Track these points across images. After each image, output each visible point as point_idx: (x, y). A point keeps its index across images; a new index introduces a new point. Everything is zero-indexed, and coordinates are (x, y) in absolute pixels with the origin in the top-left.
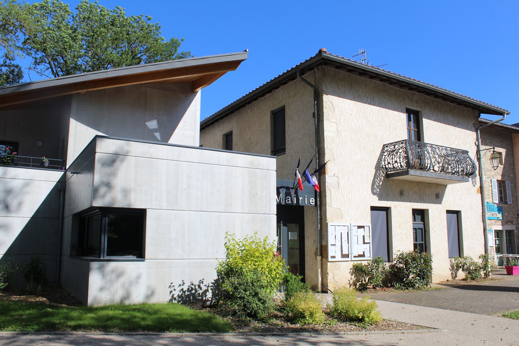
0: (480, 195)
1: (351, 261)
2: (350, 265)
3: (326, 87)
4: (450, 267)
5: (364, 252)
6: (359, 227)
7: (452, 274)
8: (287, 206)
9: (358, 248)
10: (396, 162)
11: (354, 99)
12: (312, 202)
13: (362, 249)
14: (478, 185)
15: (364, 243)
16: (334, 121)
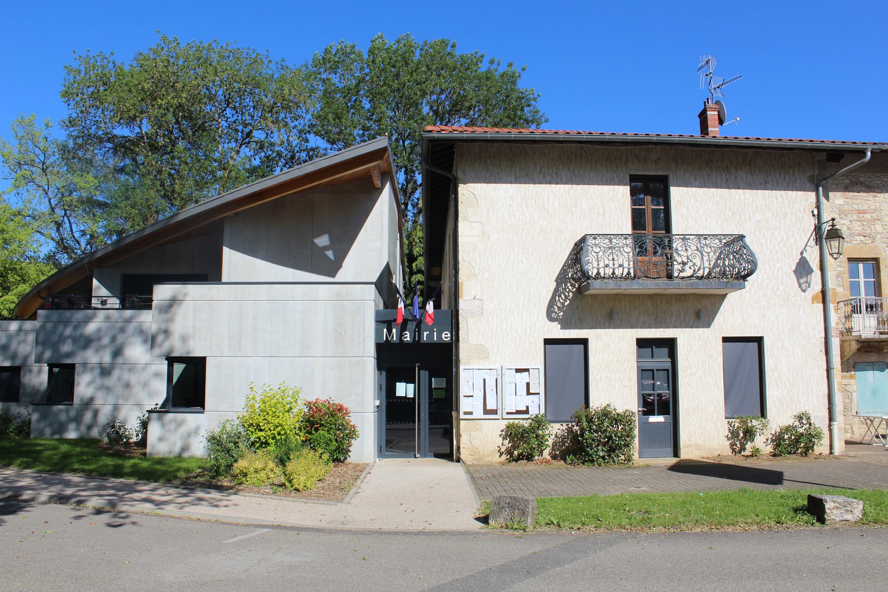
0: (821, 305)
2: (503, 424)
3: (464, 173)
4: (727, 433)
5: (527, 407)
6: (518, 371)
7: (732, 445)
9: (515, 401)
10: (620, 266)
11: (517, 181)
15: (528, 393)
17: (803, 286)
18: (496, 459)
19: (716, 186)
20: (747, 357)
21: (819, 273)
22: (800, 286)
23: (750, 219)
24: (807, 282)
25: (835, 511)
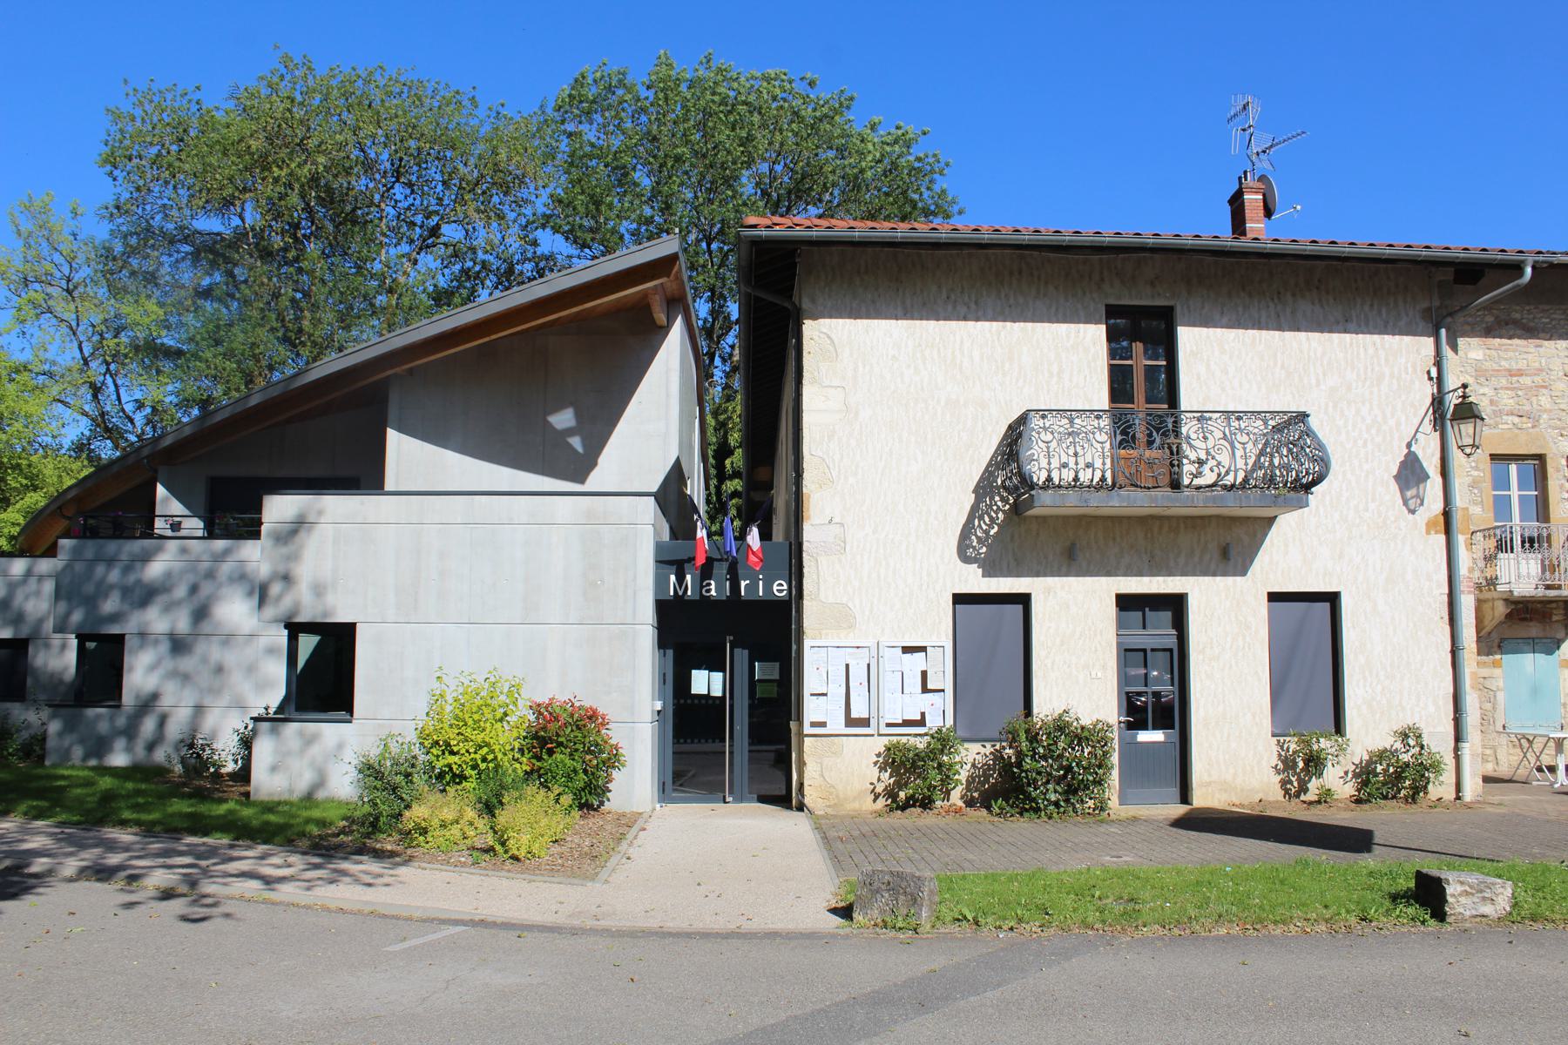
2: (880, 744)
3: (813, 301)
4: (1274, 760)
5: (923, 714)
6: (907, 650)
7: (1284, 783)
8: (679, 599)
9: (900, 703)
10: (1088, 465)
11: (907, 314)
13: (916, 699)
14: (1434, 504)
15: (925, 690)
16: (835, 383)
17: (1412, 503)
18: (868, 804)
19: (1384, 329)
20: (1311, 628)
21: (1439, 480)
22: (1405, 503)
23: (1318, 384)
24: (1417, 496)
25: (1463, 900)
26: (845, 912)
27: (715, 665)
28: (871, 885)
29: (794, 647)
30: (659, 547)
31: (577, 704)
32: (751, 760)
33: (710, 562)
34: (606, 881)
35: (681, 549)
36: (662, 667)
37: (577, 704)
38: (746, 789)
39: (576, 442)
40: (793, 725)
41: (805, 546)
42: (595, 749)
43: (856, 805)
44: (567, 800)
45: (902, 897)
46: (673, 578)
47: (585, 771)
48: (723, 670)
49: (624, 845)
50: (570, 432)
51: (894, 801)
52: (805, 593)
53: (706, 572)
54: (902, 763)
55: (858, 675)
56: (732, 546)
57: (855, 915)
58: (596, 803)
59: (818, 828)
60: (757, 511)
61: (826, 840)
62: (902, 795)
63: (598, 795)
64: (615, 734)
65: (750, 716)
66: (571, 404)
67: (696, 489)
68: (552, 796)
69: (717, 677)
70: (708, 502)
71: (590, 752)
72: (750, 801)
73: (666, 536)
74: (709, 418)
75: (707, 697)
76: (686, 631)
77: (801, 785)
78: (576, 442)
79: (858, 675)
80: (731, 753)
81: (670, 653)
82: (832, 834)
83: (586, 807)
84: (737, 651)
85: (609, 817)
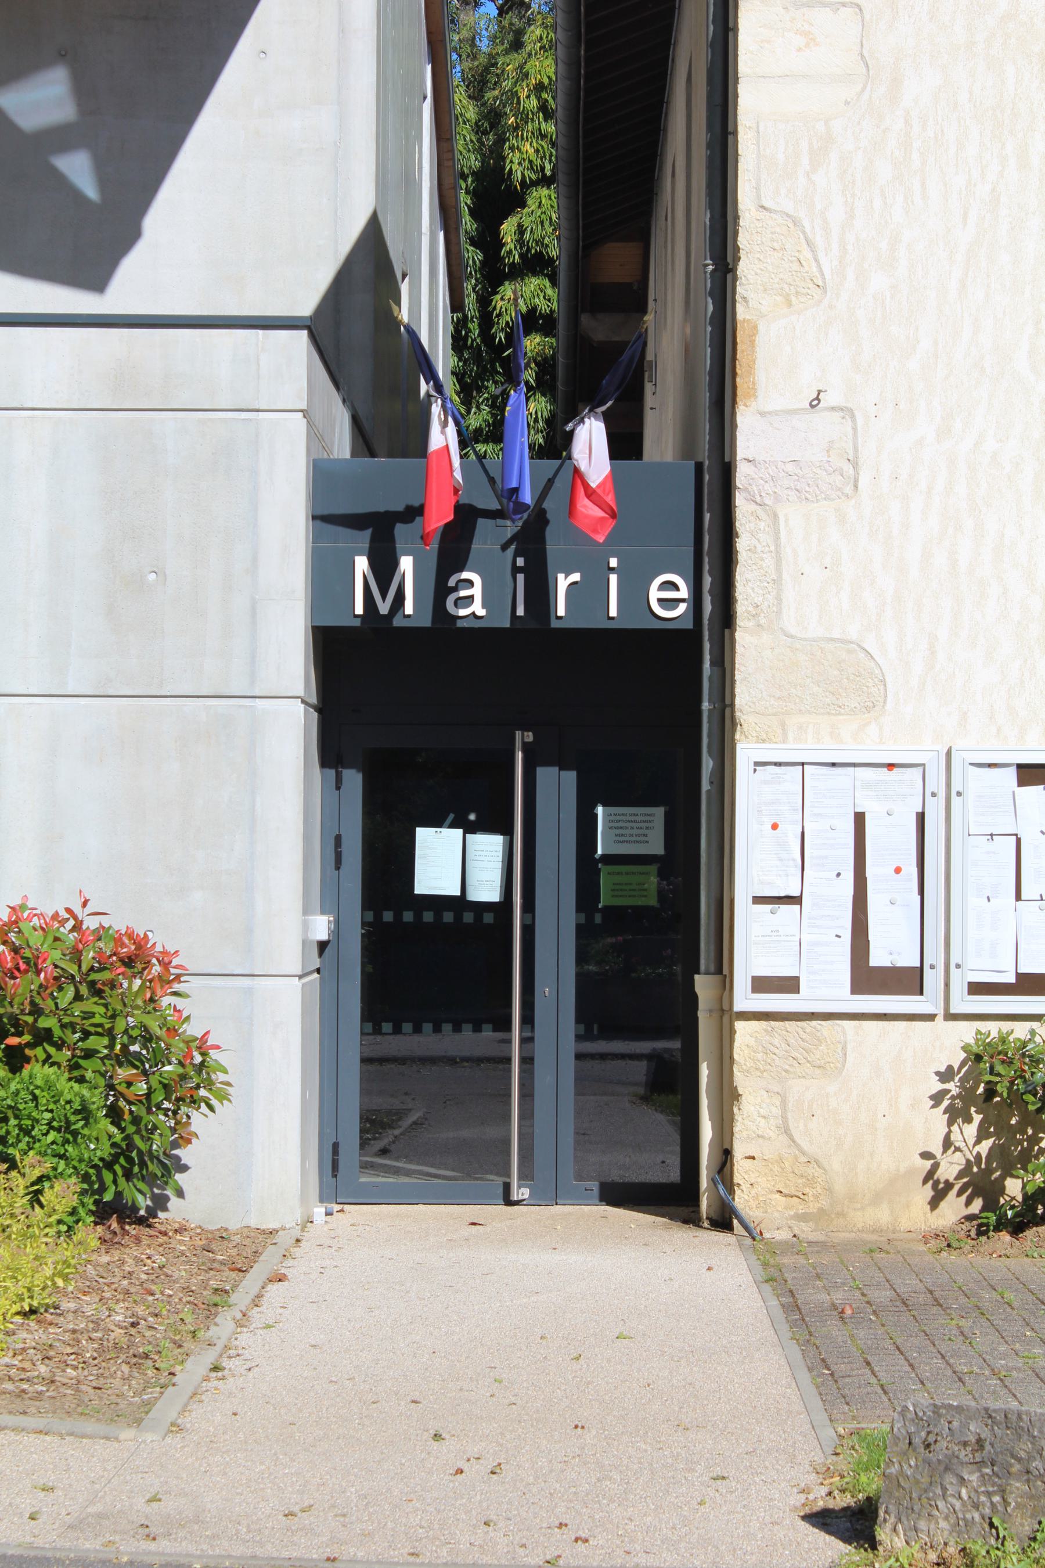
1: (950, 1017)
2: (950, 1044)
8: (377, 628)
12: (668, 603)
18: (915, 1214)
26: (855, 1524)
27: (481, 808)
28: (929, 1447)
29: (708, 764)
30: (322, 476)
31: (91, 923)
32: (581, 1081)
33: (466, 518)
34: (175, 1428)
35: (385, 484)
36: (331, 815)
37: (91, 923)
38: (568, 1168)
39: (78, 169)
40: (703, 985)
41: (742, 474)
42: (145, 1049)
43: (882, 1215)
44: (63, 1194)
45: (1018, 1486)
46: (362, 564)
47: (114, 1114)
48: (500, 824)
49: (223, 1326)
50: (59, 138)
51: (991, 1205)
52: (742, 608)
53: (452, 552)
54: (1016, 1100)
55: (890, 844)
56: (525, 476)
57: (882, 1534)
58: (143, 1203)
59: (773, 1278)
60: (600, 372)
61: (796, 1314)
62: (1014, 1187)
63: (151, 1180)
64: (200, 1009)
65: (581, 957)
66: (62, 55)
67: (425, 307)
68: (20, 1183)
69: (489, 847)
70: (459, 343)
71: (126, 1058)
72: (579, 1199)
73: (341, 444)
74: (460, 98)
75: (459, 903)
76: (404, 721)
77: (725, 1156)
78: (78, 169)
79: (890, 844)
80: (527, 1061)
81: (354, 779)
82: (813, 1296)
83: (116, 1213)
84: (546, 775)
85: (181, 1243)
